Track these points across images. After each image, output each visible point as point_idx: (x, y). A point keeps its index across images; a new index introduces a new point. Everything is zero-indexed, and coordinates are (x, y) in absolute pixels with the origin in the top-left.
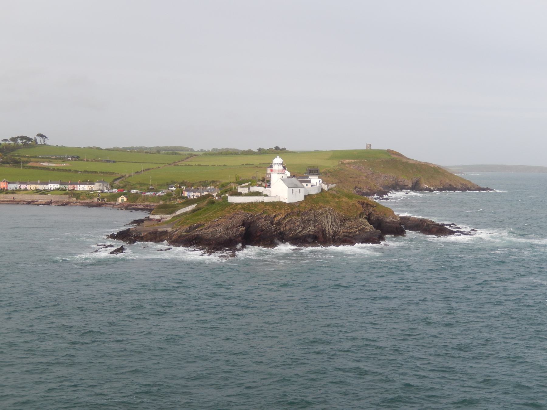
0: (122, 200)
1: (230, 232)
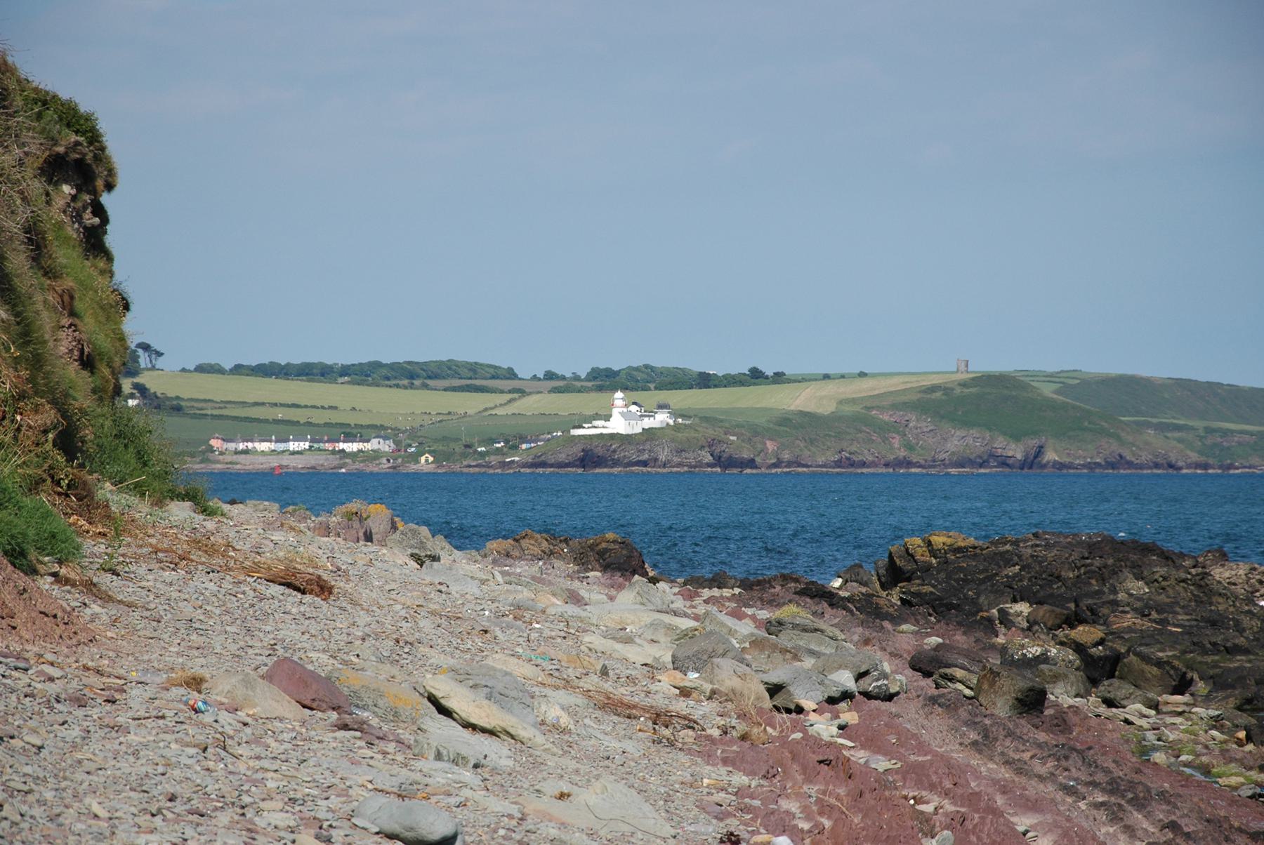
0: (427, 460)
1: (570, 458)
